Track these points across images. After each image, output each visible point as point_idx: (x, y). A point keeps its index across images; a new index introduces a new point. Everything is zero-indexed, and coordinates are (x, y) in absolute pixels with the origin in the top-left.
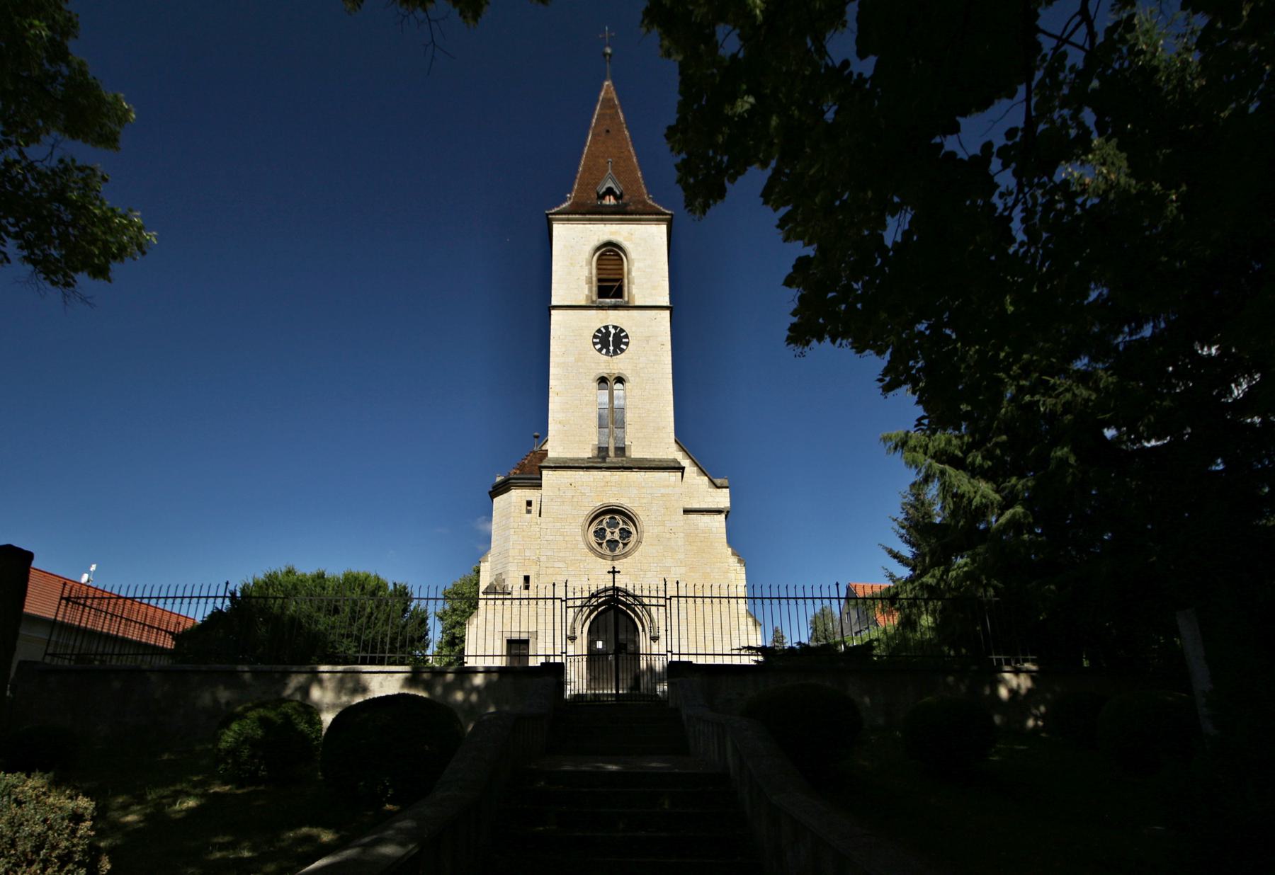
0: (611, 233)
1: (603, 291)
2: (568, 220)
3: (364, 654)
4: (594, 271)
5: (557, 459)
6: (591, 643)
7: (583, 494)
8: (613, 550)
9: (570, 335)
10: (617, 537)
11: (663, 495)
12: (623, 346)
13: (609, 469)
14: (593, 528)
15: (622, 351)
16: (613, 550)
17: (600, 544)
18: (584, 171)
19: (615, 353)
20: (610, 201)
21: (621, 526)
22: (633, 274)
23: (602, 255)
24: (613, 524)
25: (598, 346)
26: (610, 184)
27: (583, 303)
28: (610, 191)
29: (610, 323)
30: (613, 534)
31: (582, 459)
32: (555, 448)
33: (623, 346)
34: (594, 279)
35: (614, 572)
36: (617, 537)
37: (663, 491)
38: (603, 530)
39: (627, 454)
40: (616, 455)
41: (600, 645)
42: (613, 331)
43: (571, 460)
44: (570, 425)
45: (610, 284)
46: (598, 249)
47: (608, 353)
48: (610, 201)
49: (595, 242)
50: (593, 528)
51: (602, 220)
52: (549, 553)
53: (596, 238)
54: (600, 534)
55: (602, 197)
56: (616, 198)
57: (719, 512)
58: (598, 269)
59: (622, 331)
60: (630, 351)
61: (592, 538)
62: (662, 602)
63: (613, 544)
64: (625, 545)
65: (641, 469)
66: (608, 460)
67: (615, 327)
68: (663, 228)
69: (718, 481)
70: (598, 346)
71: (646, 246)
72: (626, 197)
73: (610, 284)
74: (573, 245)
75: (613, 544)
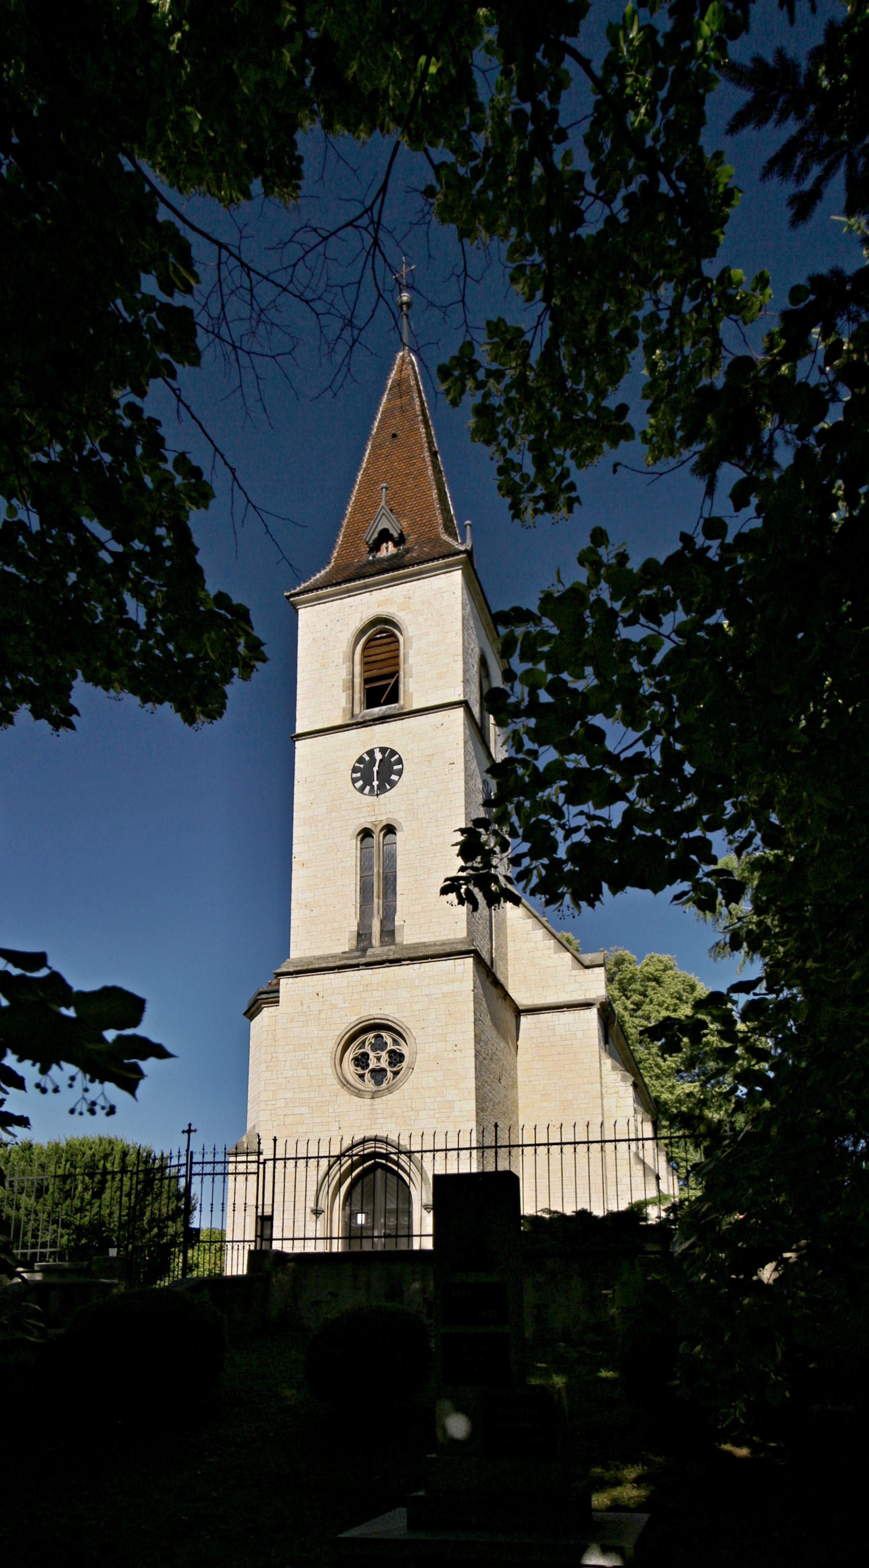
0: (380, 604)
1: (373, 698)
2: (319, 598)
3: (43, 1250)
4: (358, 669)
5: (301, 960)
6: (350, 1218)
7: (334, 1006)
8: (378, 1083)
9: (321, 771)
10: (384, 1064)
11: (445, 995)
12: (394, 777)
13: (368, 965)
14: (350, 1054)
15: (393, 784)
16: (378, 1083)
17: (362, 1076)
18: (354, 513)
19: (382, 789)
20: (388, 550)
21: (390, 1046)
22: (411, 660)
23: (369, 640)
24: (379, 1045)
25: (360, 783)
26: (384, 524)
27: (339, 722)
28: (385, 536)
29: (376, 744)
30: (379, 1060)
31: (334, 956)
32: (302, 946)
33: (394, 777)
34: (358, 680)
35: (189, 1131)
36: (384, 1064)
37: (446, 988)
38: (365, 1056)
39: (398, 939)
40: (383, 943)
41: (361, 1219)
42: (378, 756)
43: (319, 958)
44: (321, 908)
45: (380, 688)
46: (362, 632)
47: (372, 792)
48: (388, 550)
49: (357, 621)
50: (350, 1054)
51: (366, 586)
52: (289, 1095)
53: (358, 616)
54: (361, 1061)
55: (375, 547)
56: (396, 544)
57: (588, 1005)
58: (365, 664)
59: (393, 753)
60: (405, 783)
61: (349, 1069)
62: (253, 1167)
63: (378, 1074)
64: (396, 1074)
65: (413, 959)
66: (370, 952)
67: (383, 750)
68: (457, 577)
69: (587, 958)
70: (360, 783)
71: (434, 614)
72: (411, 538)
73: (380, 688)
74: (325, 635)
75: (378, 1074)
